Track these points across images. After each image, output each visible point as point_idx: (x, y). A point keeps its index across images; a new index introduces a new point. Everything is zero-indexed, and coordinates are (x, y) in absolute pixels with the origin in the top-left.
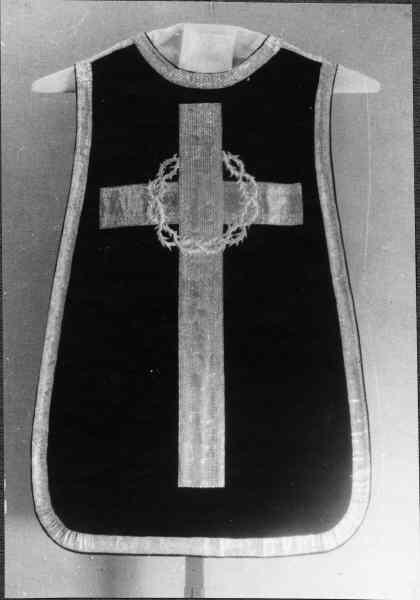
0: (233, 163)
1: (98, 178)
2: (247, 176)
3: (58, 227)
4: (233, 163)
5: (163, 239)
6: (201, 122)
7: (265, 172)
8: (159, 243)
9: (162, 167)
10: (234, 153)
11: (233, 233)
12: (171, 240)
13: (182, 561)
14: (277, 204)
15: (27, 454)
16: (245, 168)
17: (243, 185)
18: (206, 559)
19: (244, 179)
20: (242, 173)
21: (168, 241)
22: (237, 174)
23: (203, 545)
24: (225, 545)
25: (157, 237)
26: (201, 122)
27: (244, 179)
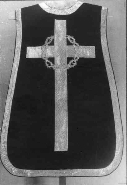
0: (71, 39)
1: (99, 59)
2: (77, 44)
3: (1, 119)
4: (71, 39)
5: (47, 65)
6: (60, 26)
7: (82, 42)
8: (46, 67)
9: (47, 40)
10: (71, 36)
11: (72, 63)
12: (50, 65)
13: (58, 179)
14: (89, 52)
15: (1, 119)
16: (75, 41)
17: (74, 46)
18: (66, 178)
19: (75, 45)
20: (74, 42)
21: (49, 66)
22: (72, 42)
23: (65, 172)
24: (76, 172)
25: (45, 65)
26: (60, 26)
27: (75, 45)
